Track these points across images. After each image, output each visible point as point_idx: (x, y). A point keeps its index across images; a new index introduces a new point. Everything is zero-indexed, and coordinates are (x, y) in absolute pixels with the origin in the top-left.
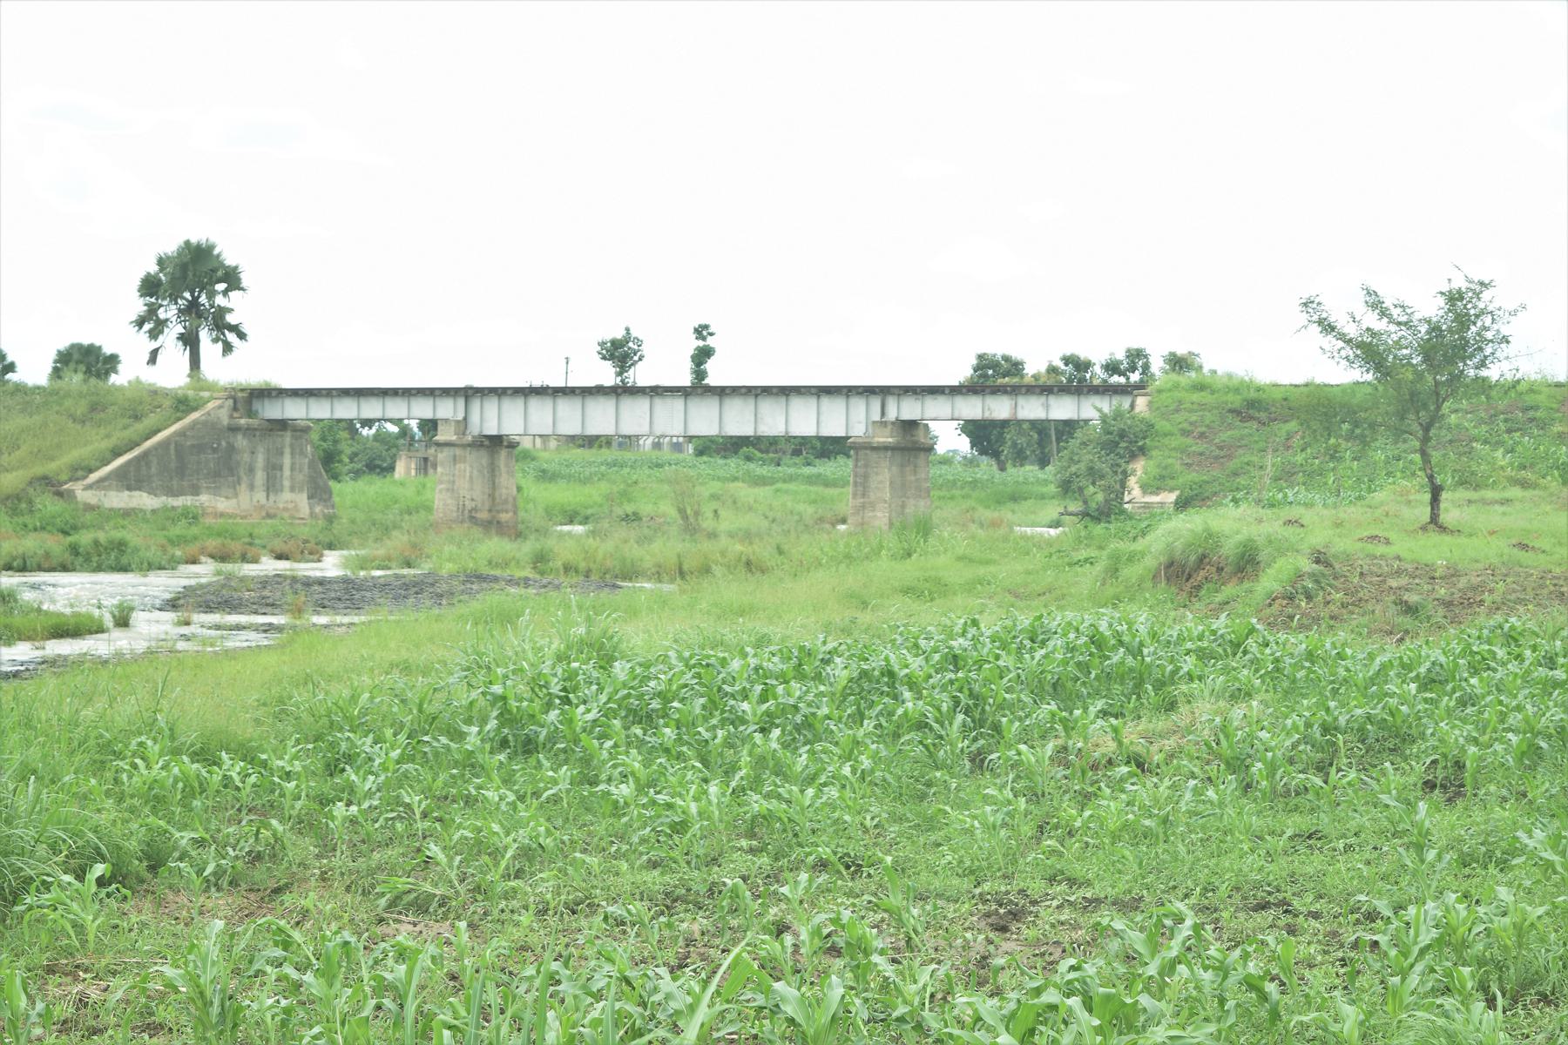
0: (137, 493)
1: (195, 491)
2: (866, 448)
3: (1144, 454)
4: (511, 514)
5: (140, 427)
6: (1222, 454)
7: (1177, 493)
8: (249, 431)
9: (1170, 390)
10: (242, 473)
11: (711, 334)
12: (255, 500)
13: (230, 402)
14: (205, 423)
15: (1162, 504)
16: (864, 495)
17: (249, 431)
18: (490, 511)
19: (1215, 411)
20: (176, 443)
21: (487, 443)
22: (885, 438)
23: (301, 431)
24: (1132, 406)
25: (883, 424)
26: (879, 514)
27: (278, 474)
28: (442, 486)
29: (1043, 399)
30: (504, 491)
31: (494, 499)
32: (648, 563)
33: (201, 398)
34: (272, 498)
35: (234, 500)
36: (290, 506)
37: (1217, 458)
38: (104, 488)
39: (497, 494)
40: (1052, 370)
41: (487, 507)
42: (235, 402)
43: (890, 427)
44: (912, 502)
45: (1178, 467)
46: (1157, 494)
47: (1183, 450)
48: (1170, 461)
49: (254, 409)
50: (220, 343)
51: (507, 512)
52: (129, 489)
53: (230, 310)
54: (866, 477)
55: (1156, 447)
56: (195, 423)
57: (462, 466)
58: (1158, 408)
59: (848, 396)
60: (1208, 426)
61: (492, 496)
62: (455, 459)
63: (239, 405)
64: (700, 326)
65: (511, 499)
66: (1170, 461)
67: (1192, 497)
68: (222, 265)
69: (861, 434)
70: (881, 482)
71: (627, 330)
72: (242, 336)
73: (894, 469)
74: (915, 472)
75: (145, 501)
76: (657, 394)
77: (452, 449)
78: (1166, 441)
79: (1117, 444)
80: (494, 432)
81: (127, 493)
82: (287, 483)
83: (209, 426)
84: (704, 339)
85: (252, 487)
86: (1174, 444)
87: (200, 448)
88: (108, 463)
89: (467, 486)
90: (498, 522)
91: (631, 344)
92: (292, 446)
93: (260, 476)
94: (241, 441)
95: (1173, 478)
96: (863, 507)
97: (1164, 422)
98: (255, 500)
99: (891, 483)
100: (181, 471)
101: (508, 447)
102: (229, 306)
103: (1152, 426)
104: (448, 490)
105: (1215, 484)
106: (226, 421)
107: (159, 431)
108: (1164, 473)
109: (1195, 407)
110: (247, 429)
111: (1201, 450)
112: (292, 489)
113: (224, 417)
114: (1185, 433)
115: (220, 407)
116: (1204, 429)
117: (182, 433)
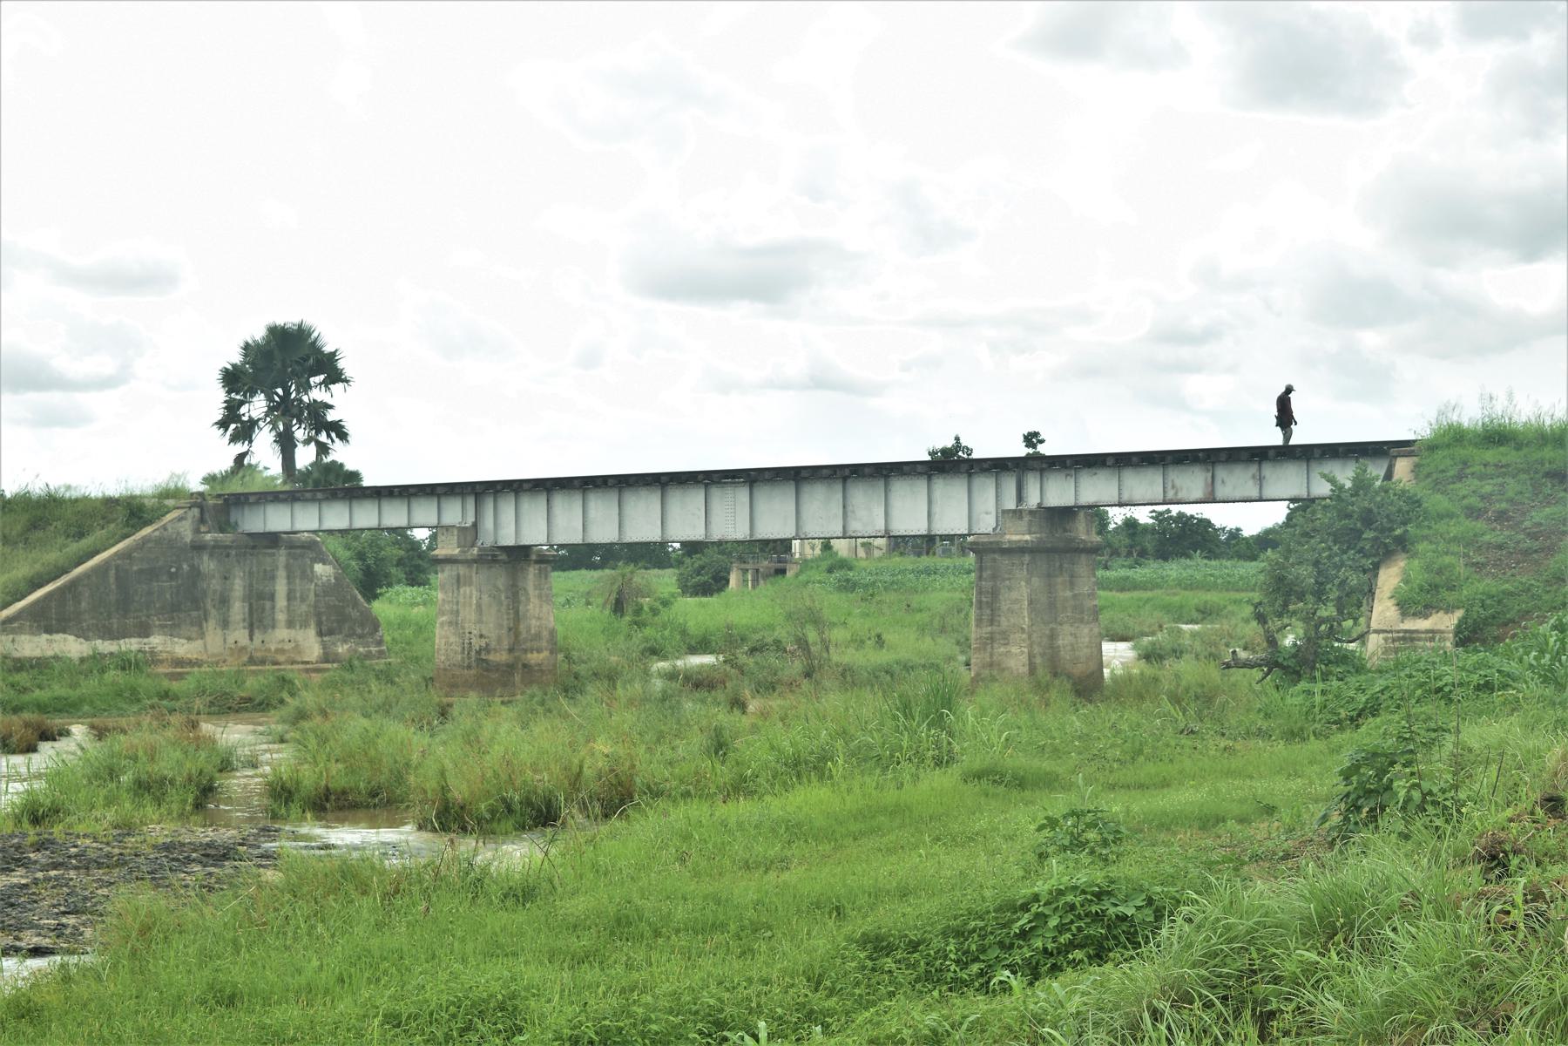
0: (58, 637)
1: (144, 631)
2: (993, 551)
3: (1405, 550)
4: (546, 654)
5: (86, 543)
6: (1536, 545)
7: (1459, 613)
8: (217, 550)
9: (1448, 446)
10: (209, 606)
11: (1042, 442)
12: (231, 640)
13: (196, 511)
14: (159, 541)
15: (1432, 633)
16: (992, 622)
17: (217, 550)
18: (511, 650)
19: (1523, 477)
20: (117, 567)
21: (503, 557)
22: (1019, 535)
23: (303, 547)
24: (1389, 476)
25: (1017, 514)
26: (1015, 650)
27: (268, 604)
28: (444, 618)
29: (1253, 469)
30: (534, 622)
31: (517, 635)
32: (422, 780)
33: (166, 506)
34: (258, 637)
35: (200, 642)
36: (288, 646)
37: (1527, 553)
38: (14, 631)
39: (522, 627)
41: (505, 645)
42: (202, 513)
43: (1027, 518)
44: (1067, 628)
45: (1461, 569)
46: (1426, 617)
47: (1471, 542)
48: (1447, 559)
49: (232, 520)
50: (313, 443)
51: (539, 651)
52: (49, 631)
53: (331, 407)
54: (994, 594)
55: (1425, 538)
56: (145, 540)
57: (468, 590)
58: (1428, 475)
59: (970, 475)
60: (1511, 501)
61: (514, 630)
62: (459, 581)
63: (207, 516)
64: (1030, 434)
65: (545, 633)
66: (1447, 559)
67: (1485, 621)
68: (319, 351)
69: (990, 530)
70: (1016, 601)
71: (957, 439)
72: (343, 436)
73: (1036, 581)
74: (1072, 585)
75: (72, 647)
76: (713, 482)
77: (455, 567)
78: (1441, 527)
79: (1358, 534)
80: (510, 542)
81: (45, 636)
82: (281, 617)
83: (166, 544)
84: (1034, 446)
85: (225, 624)
86: (1454, 532)
87: (152, 574)
88: (23, 597)
89: (473, 617)
90: (525, 666)
91: (960, 453)
92: (288, 567)
93: (238, 609)
94: (208, 564)
95: (1451, 588)
96: (992, 639)
97: (1439, 497)
98: (231, 640)
99: (1031, 602)
100: (124, 604)
101: (537, 562)
102: (330, 402)
103: (1418, 503)
104: (450, 623)
105: (1524, 597)
106: (188, 536)
107: (97, 552)
108: (1437, 579)
109: (1490, 470)
110: (214, 547)
111: (1500, 540)
112: (290, 624)
113: (186, 531)
114: (1473, 513)
115: (180, 519)
116: (1504, 505)
117: (126, 555)
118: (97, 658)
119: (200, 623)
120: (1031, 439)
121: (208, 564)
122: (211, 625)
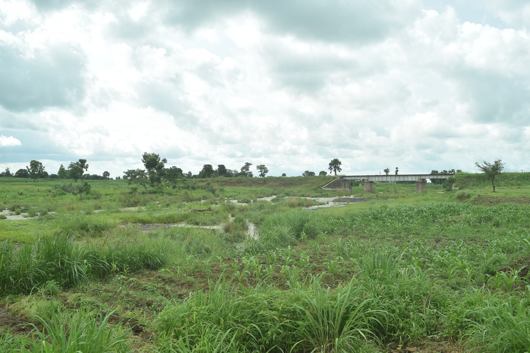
8: (342, 181)
32: (391, 196)
40: (442, 172)
47: (460, 182)
75: (330, 189)
83: (337, 180)
93: (343, 186)
94: (341, 182)
114: (460, 180)
117: (334, 181)
118: (332, 190)
119: (340, 187)
120: (387, 171)
121: (341, 182)
122: (341, 188)
